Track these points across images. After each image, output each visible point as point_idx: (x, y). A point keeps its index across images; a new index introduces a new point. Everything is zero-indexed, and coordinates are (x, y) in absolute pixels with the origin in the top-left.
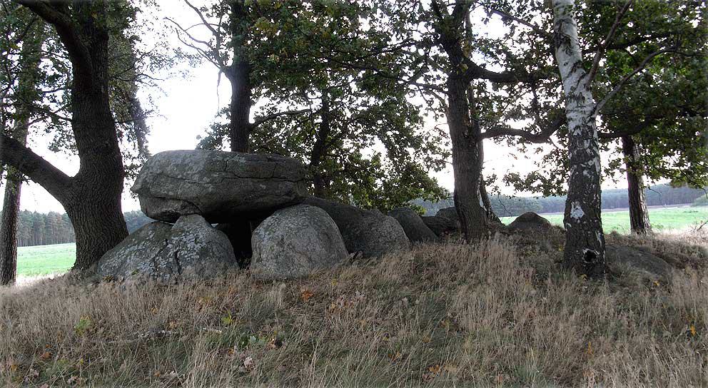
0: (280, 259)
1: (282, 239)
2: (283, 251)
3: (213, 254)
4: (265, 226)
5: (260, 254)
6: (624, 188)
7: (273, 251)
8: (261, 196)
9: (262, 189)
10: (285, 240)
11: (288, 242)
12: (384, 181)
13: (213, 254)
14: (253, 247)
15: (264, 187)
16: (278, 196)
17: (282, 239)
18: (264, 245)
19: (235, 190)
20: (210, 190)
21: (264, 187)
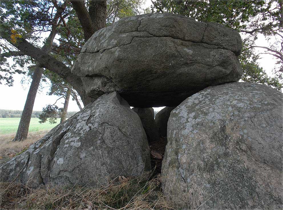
0: (220, 174)
1: (223, 129)
2: (226, 155)
3: (103, 142)
4: (190, 104)
5: (177, 154)
6: (20, 110)
7: (202, 151)
8: (186, 64)
9: (187, 54)
10: (228, 131)
11: (235, 136)
12: (90, 127)
13: (103, 142)
14: (169, 136)
15: (190, 52)
16: (210, 66)
17: (223, 129)
18: (186, 137)
19: (149, 54)
20: (117, 54)
21: (190, 52)
